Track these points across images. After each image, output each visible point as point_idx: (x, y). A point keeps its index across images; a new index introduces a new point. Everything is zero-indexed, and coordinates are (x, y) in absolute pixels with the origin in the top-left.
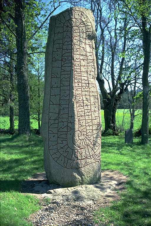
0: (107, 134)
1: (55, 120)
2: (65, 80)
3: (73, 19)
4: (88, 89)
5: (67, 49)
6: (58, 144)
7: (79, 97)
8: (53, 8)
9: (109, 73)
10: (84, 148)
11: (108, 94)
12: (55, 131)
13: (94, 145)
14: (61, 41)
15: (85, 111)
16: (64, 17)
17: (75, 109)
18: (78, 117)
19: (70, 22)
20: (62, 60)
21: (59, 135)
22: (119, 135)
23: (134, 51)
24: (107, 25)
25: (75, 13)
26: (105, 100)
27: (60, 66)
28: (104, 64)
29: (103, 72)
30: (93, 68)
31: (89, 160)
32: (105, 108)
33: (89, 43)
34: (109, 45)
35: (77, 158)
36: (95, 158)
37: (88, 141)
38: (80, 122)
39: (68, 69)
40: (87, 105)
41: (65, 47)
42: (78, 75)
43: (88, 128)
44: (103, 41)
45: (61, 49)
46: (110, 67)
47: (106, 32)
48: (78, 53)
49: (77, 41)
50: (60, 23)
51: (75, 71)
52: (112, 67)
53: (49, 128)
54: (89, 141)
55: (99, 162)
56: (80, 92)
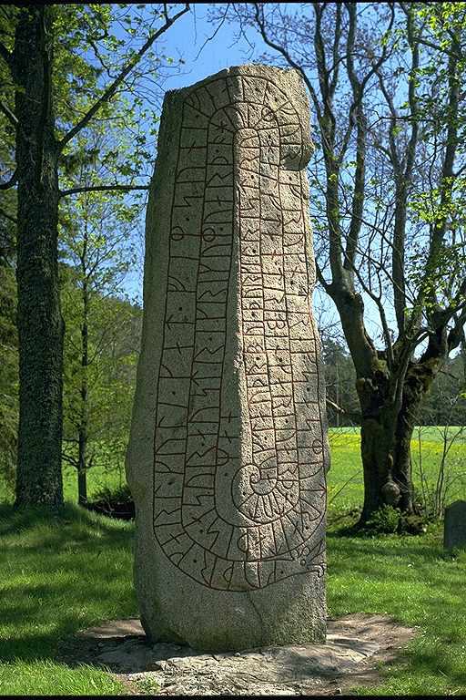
0: (373, 526)
1: (176, 428)
2: (212, 299)
3: (240, 105)
4: (286, 331)
5: (219, 201)
6: (184, 507)
7: (255, 355)
8: (162, 22)
9: (382, 267)
10: (270, 522)
11: (381, 355)
12: (176, 463)
13: (302, 512)
14: (200, 175)
15: (275, 399)
16: (212, 98)
17: (243, 393)
18: (251, 418)
19: (229, 114)
20: (202, 235)
21: (188, 478)
22: (425, 530)
24: (376, 68)
25: (245, 84)
26: (368, 383)
27: (196, 255)
28: (363, 230)
29: (357, 265)
30: (303, 259)
32: (365, 418)
33: (290, 179)
34: (383, 149)
35: (247, 552)
36: (305, 558)
37: (282, 500)
38: (258, 437)
39: (221, 264)
40: (281, 383)
41: (211, 194)
42: (254, 283)
44: (361, 133)
45: (201, 200)
46: (386, 244)
47: (374, 97)
49: (253, 174)
50: (197, 116)
52: (398, 246)
53: (155, 454)
54: (287, 499)
56: (259, 339)
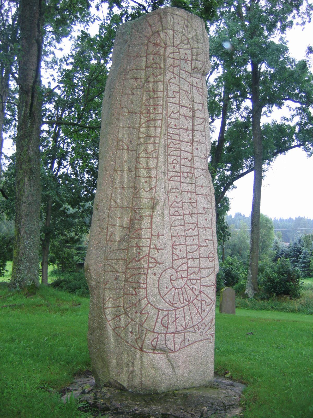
12: (121, 266)
23: (81, 90)
30: (204, 135)
31: (190, 334)
43: (191, 263)
48: (176, 100)
49: (176, 76)
51: (169, 137)
55: (210, 339)
